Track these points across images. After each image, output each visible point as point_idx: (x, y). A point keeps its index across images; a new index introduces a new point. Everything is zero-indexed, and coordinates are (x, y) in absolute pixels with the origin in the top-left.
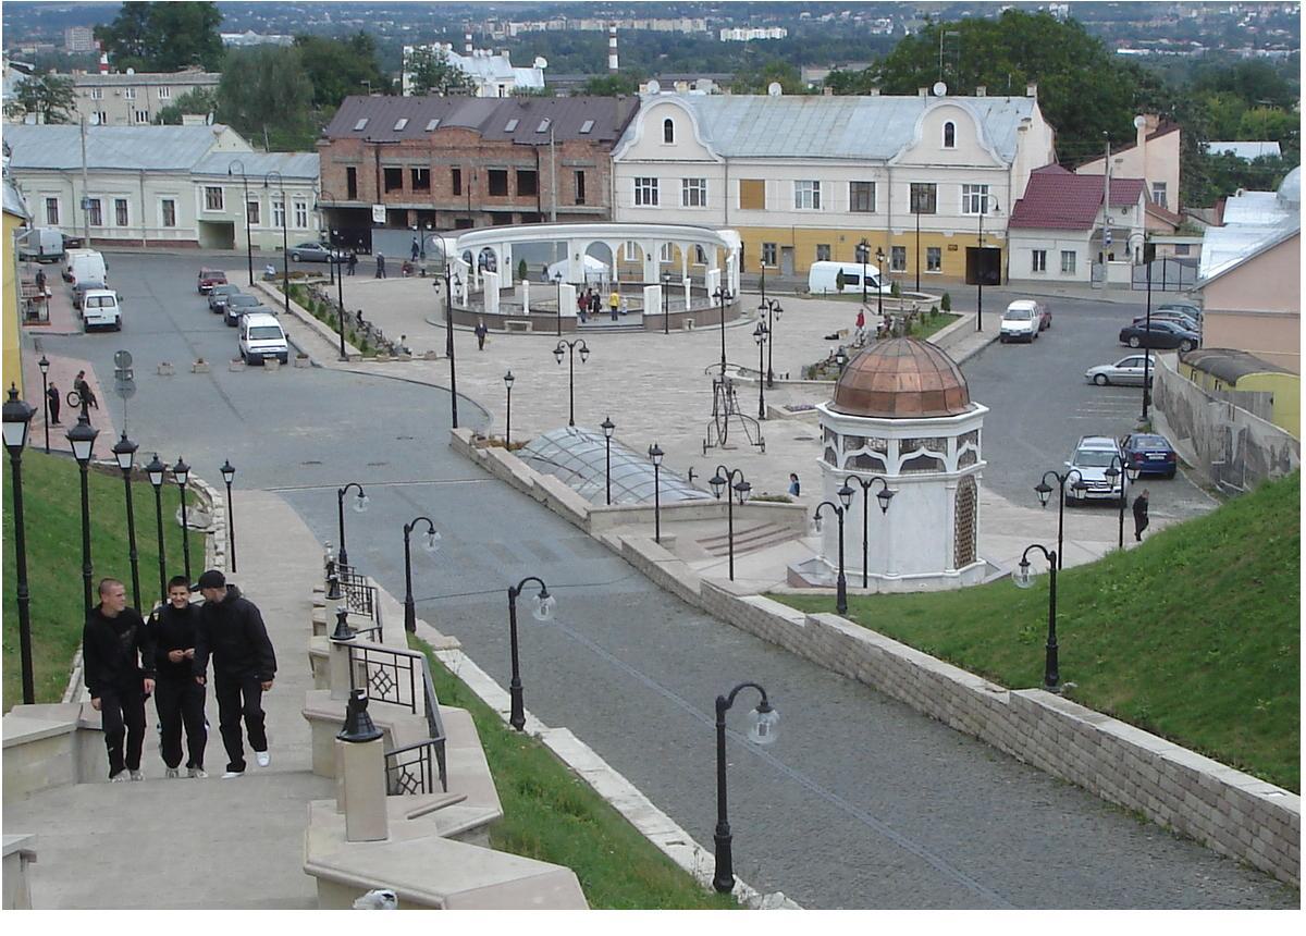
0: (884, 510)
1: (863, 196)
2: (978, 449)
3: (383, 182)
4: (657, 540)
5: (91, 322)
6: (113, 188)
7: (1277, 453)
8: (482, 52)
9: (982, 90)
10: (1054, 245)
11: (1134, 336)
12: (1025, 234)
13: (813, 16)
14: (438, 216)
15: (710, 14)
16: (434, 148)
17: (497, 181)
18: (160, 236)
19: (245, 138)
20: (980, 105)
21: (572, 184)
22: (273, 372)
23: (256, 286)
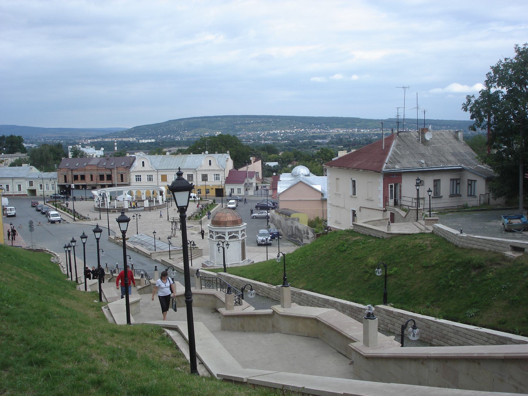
0: (228, 248)
1: (190, 178)
2: (245, 233)
3: (73, 178)
4: (170, 259)
5: (8, 215)
6: (5, 182)
7: (305, 231)
8: (88, 147)
9: (216, 152)
10: (236, 187)
11: (258, 207)
12: (229, 185)
13: (161, 136)
14: (87, 186)
15: (137, 137)
16: (86, 170)
17: (102, 177)
18: (17, 194)
19: (38, 169)
20: (217, 156)
21: (120, 177)
22: (57, 225)
23: (45, 204)
